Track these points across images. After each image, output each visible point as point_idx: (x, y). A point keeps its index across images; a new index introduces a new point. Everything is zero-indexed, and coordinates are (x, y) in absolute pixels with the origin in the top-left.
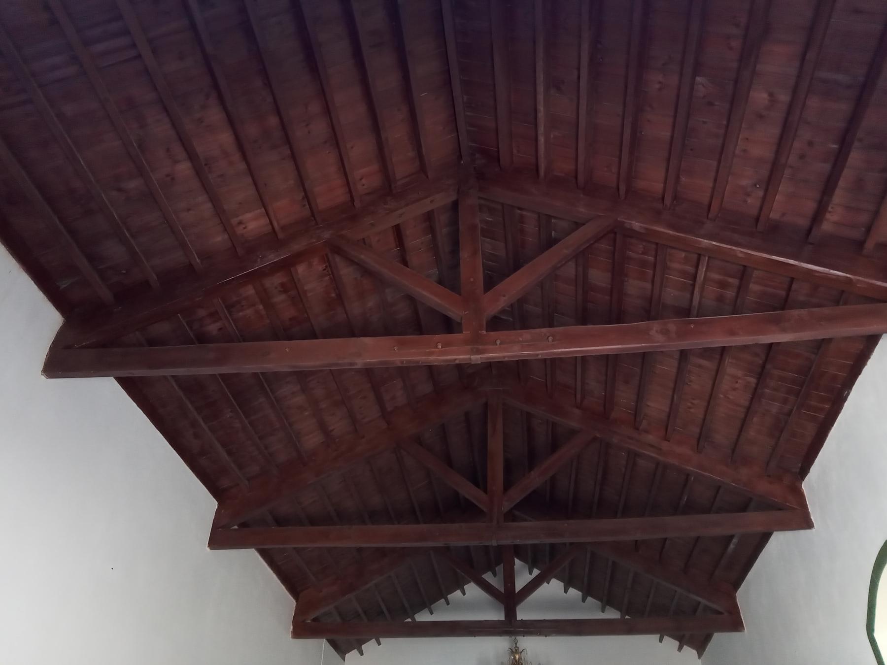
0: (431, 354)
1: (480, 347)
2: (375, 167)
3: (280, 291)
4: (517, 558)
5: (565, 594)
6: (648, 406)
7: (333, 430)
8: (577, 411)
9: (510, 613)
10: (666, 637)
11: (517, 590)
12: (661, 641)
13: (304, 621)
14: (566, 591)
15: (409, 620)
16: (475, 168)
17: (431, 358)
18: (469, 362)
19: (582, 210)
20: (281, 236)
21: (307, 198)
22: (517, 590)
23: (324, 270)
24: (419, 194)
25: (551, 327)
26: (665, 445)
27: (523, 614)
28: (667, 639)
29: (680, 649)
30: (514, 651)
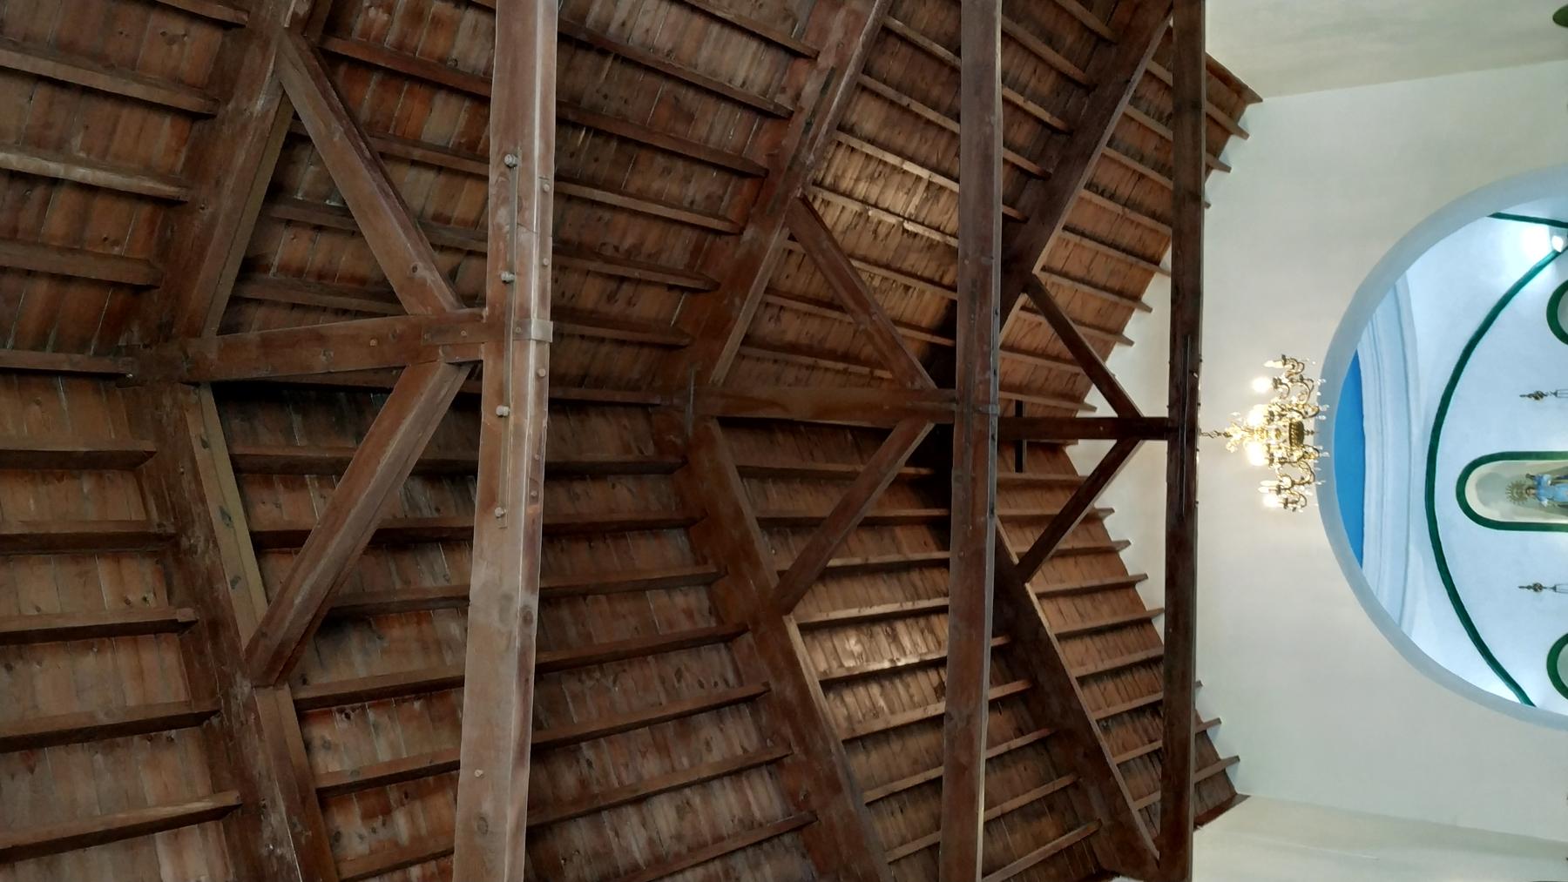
0: (519, 433)
1: (513, 319)
2: (103, 570)
3: (384, 824)
5: (1134, 346)
6: (744, 83)
7: (745, 750)
8: (748, 234)
9: (1154, 429)
11: (1113, 414)
13: (1158, 863)
14: (1130, 343)
16: (145, 346)
17: (529, 430)
18: (547, 347)
19: (259, 105)
20: (231, 798)
21: (149, 728)
22: (1113, 414)
23: (348, 717)
24: (183, 473)
25: (553, 253)
26: (826, 61)
27: (1152, 402)
29: (1243, 134)
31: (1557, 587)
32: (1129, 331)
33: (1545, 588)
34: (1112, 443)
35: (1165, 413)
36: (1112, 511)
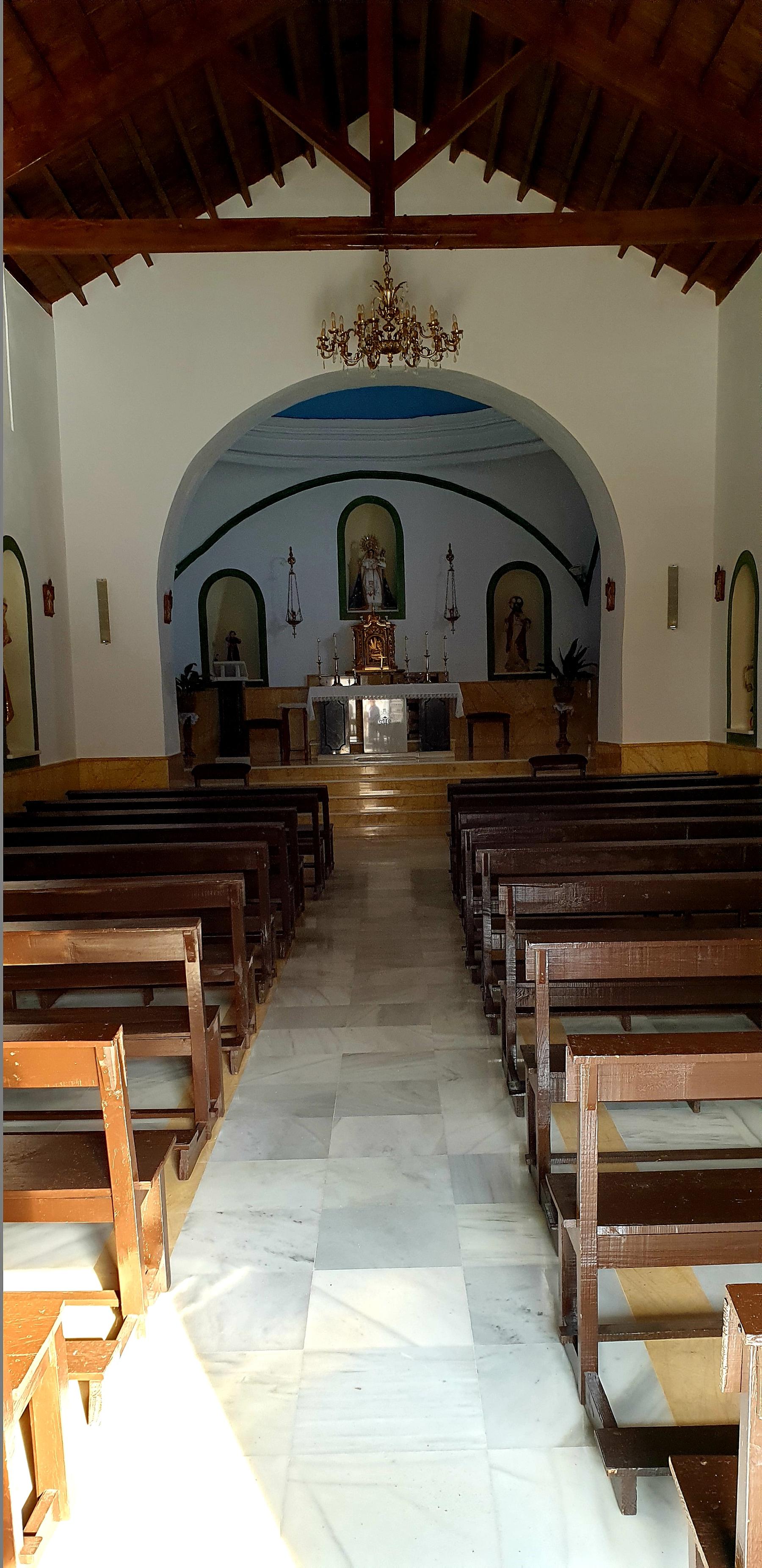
4: (399, 111)
10: (632, 249)
12: (686, 288)
15: (206, 216)
28: (633, 251)
30: (385, 283)
31: (293, 576)
32: (500, 177)
33: (292, 567)
34: (369, 158)
35: (397, 213)
36: (281, 184)
